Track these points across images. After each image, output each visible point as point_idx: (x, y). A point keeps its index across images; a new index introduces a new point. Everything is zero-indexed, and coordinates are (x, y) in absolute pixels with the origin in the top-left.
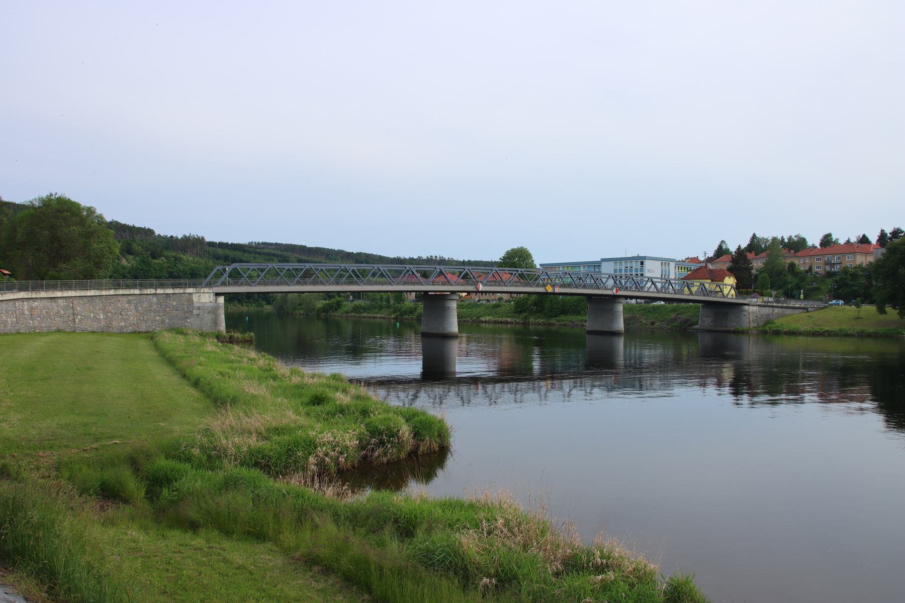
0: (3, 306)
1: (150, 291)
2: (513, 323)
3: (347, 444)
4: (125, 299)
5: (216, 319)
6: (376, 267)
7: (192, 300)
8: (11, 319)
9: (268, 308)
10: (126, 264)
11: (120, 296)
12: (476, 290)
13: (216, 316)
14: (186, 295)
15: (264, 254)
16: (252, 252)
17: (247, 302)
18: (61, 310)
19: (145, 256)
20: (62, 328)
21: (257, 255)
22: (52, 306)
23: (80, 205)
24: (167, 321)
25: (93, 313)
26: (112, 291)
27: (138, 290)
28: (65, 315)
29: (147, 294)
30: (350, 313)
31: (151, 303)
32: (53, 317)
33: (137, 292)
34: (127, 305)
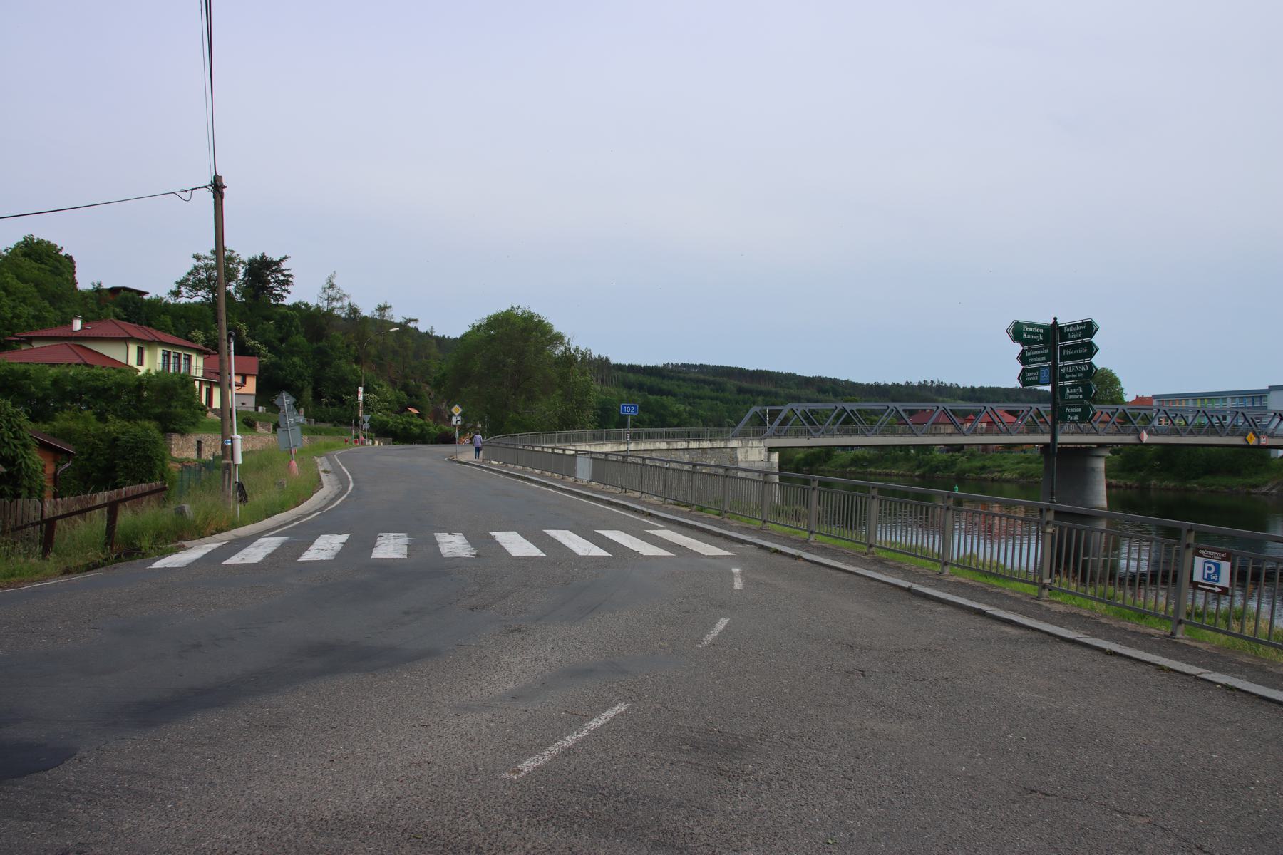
2: (1121, 487)
6: (1034, 408)
7: (737, 458)
12: (1138, 442)
14: (728, 450)
15: (691, 380)
27: (665, 444)
29: (677, 449)
30: (847, 467)
33: (664, 446)
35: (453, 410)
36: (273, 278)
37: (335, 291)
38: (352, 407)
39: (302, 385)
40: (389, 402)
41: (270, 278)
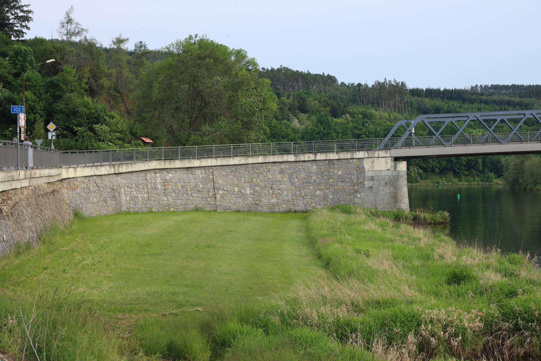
0: (133, 179)
1: (309, 157)
3: (464, 325)
4: (276, 168)
5: (395, 193)
8: (142, 195)
9: (498, 183)
10: (298, 126)
11: (270, 165)
13: (395, 188)
14: (355, 161)
16: (475, 100)
17: (467, 175)
18: (199, 184)
19: (323, 113)
20: (200, 206)
21: (483, 105)
22: (189, 179)
23: (226, 48)
24: (331, 197)
25: (237, 187)
26: (261, 157)
28: (204, 190)
29: (304, 161)
31: (310, 172)
32: (190, 193)
34: (279, 176)
35: (48, 127)
36: (12, 14)
37: (73, 26)
38: (83, 138)
39: (35, 118)
40: (121, 132)
41: (9, 14)
